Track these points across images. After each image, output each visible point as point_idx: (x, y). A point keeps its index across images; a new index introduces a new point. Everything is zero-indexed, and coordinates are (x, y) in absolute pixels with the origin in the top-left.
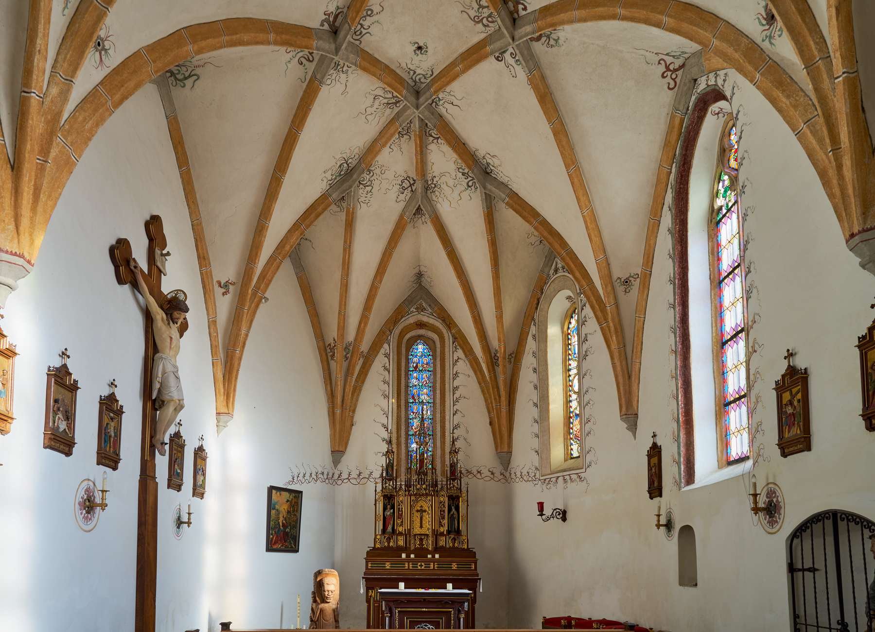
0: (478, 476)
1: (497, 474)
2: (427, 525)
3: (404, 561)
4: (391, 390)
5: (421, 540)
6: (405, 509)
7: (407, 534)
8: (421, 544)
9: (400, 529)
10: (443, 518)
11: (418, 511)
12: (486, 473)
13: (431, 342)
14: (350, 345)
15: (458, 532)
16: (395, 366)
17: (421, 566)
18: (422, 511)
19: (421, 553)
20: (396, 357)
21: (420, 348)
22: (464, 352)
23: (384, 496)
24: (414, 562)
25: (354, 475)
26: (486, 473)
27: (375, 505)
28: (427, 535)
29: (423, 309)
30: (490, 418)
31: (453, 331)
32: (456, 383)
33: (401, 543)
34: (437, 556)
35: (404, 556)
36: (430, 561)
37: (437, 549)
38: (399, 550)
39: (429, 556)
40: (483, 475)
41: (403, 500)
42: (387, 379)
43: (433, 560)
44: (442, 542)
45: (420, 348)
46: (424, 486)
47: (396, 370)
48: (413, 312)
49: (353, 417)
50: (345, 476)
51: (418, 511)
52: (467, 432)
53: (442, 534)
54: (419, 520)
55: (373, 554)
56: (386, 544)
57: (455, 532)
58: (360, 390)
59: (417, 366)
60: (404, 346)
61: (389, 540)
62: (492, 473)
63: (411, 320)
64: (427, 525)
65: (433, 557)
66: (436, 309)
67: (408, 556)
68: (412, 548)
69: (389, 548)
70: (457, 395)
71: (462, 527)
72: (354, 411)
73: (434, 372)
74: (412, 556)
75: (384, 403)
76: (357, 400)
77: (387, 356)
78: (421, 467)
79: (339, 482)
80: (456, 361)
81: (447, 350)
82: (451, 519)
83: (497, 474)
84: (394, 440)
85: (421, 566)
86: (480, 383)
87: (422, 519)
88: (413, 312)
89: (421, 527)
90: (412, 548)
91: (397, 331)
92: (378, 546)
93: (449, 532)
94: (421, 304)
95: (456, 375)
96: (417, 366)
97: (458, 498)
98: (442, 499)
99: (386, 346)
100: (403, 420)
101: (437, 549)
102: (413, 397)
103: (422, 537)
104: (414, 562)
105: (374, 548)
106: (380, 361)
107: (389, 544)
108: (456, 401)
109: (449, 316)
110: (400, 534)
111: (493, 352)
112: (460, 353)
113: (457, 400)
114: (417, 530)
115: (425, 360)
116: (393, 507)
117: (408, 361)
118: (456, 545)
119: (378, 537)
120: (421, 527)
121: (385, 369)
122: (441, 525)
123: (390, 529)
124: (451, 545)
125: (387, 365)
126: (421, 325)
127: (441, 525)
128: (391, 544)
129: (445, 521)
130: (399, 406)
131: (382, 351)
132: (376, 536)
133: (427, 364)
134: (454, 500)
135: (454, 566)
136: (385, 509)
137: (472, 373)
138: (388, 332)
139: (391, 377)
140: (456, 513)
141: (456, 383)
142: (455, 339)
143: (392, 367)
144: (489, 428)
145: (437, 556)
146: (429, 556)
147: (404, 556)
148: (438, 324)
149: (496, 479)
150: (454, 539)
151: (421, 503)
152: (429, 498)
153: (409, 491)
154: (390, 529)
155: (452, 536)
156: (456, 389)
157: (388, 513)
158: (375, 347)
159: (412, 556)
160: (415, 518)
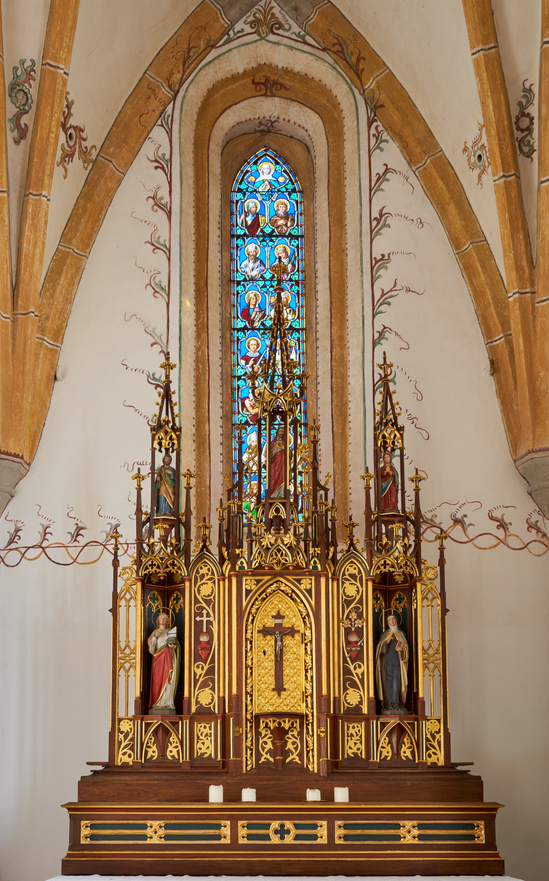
0: (457, 532)
1: (518, 527)
2: (296, 679)
3: (218, 814)
4: (178, 272)
5: (280, 734)
6: (221, 627)
7: (227, 717)
8: (280, 750)
9: (205, 697)
10: (358, 657)
11: (265, 632)
12: (479, 522)
13: (298, 150)
14: (29, 73)
15: (412, 704)
16: (190, 198)
17: (282, 832)
18: (279, 631)
19: (281, 782)
20: (190, 171)
21: (266, 172)
22: (405, 147)
23: (146, 582)
24: (256, 818)
25: (60, 533)
26: (479, 522)
27: (114, 611)
28: (302, 717)
29: (275, 26)
30: (492, 350)
31: (370, 84)
32: (381, 246)
33: (207, 746)
34: (341, 795)
35: (216, 794)
36: (314, 814)
37: (338, 768)
38: (202, 771)
39: (313, 795)
40: (472, 532)
41: (205, 587)
42: (164, 237)
43: (328, 811)
44: (353, 745)
45: (266, 172)
46: (289, 539)
47: (190, 211)
48: (241, 34)
49: (54, 353)
50: (30, 536)
51: (265, 632)
52: (420, 396)
53: (354, 714)
54: (270, 664)
55: (102, 784)
56: (153, 752)
57: (401, 703)
58: (79, 270)
59: (256, 222)
60: (215, 148)
61: (162, 735)
62: (502, 525)
63: (237, 58)
64: (296, 679)
65: (328, 797)
66: (314, 18)
67: (232, 796)
68: (248, 762)
69: (164, 766)
70: (384, 282)
71: (427, 688)
72: (58, 334)
73: (306, 239)
74: (248, 795)
75: (154, 310)
76: (69, 301)
77: (163, 165)
78: (276, 480)
79: (13, 557)
80: (381, 178)
81: (349, 147)
82: (385, 657)
83: (518, 527)
84: (186, 419)
85: (282, 832)
86: (455, 243)
87: (284, 658)
88: (241, 34)
89: (279, 688)
90: (248, 762)
91: (194, 91)
92: (123, 758)
93: (379, 707)
94: (267, 11)
95: (380, 220)
96: (256, 222)
97: (411, 582)
98: (351, 590)
99: (158, 134)
100: (216, 372)
101: (338, 768)
102: (246, 314)
103: (282, 725)
104: (256, 818)
105: (110, 768)
106: (140, 181)
107: (163, 749)
108: (380, 302)
109: (356, 34)
110: (204, 714)
111: (515, 95)
112: (391, 154)
113: (385, 299)
114: (265, 700)
115: (281, 205)
116: (178, 622)
117: (229, 208)
118: (406, 752)
119: (125, 726)
120: (279, 688)
121: (158, 204)
122: (349, 681)
123: (166, 697)
124: (387, 752)
125: (163, 192)
126: (266, 81)
127: (349, 681)
128: (172, 751)
129: (365, 669)
130: (202, 328)
131: (147, 150)
132: (115, 720)
133: (286, 216)
134: (394, 590)
135: (409, 833)
136: (149, 629)
137: (429, 213)
138: (165, 92)
139: (177, 231)
140: (401, 638)
141: (381, 246)
142: (375, 108)
143: (181, 199)
144: (488, 385)
145: (341, 795)
146: (313, 795)
147: (216, 794)
148: (321, 69)
149: (513, 542)
150: (400, 730)
151: (279, 603)
152: (307, 583)
153: (233, 559)
154: (166, 697)
155: (393, 722)
156: (379, 263)
157: (161, 639)
158: (126, 134)
159: (248, 795)
160: (255, 656)
